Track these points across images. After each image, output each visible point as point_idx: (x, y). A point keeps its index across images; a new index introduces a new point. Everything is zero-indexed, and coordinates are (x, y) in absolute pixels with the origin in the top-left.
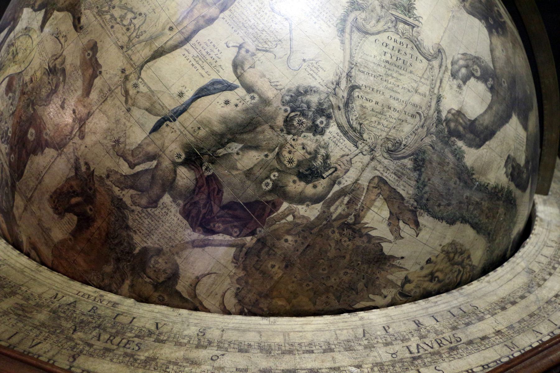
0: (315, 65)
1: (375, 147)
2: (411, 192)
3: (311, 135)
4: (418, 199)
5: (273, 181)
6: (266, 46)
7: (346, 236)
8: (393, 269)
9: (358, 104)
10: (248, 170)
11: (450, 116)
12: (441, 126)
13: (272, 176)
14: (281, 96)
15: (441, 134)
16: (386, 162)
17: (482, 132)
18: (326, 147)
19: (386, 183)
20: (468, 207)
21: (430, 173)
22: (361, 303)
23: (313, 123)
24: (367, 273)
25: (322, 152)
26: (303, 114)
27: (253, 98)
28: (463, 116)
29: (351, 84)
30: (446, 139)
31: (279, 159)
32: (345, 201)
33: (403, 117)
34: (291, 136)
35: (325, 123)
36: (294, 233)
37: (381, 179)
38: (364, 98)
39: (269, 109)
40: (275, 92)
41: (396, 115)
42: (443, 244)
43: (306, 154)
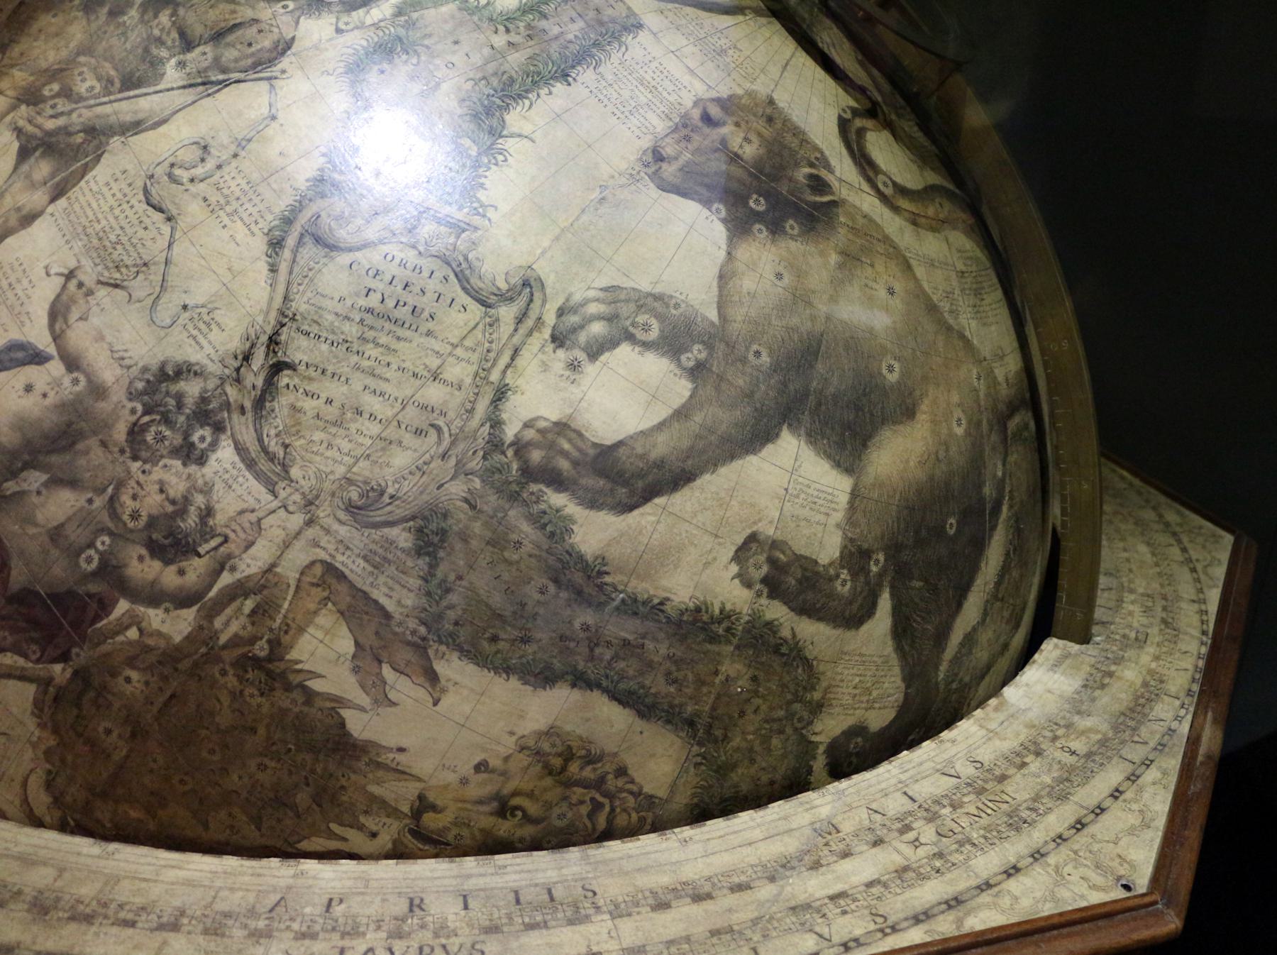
0: (206, 318)
1: (317, 497)
2: (409, 602)
3: (177, 463)
4: (431, 621)
5: (101, 554)
6: (117, 275)
7: (252, 684)
8: (380, 773)
9: (284, 403)
10: (56, 528)
11: (530, 434)
12: (498, 457)
13: (98, 544)
14: (127, 381)
15: (497, 476)
16: (343, 531)
17: (641, 475)
18: (207, 490)
19: (341, 576)
20: (592, 650)
21: (462, 563)
22: (313, 839)
23: (185, 439)
24: (313, 771)
25: (199, 500)
26: (167, 420)
27: (75, 382)
28: (573, 435)
29: (274, 360)
30: (514, 487)
31: (114, 510)
32: (247, 610)
33: (391, 432)
34: (138, 464)
35: (209, 439)
36: (141, 666)
37: (330, 568)
38: (301, 390)
39: (103, 407)
40: (119, 371)
41: (375, 429)
42: (520, 732)
43: (167, 503)
